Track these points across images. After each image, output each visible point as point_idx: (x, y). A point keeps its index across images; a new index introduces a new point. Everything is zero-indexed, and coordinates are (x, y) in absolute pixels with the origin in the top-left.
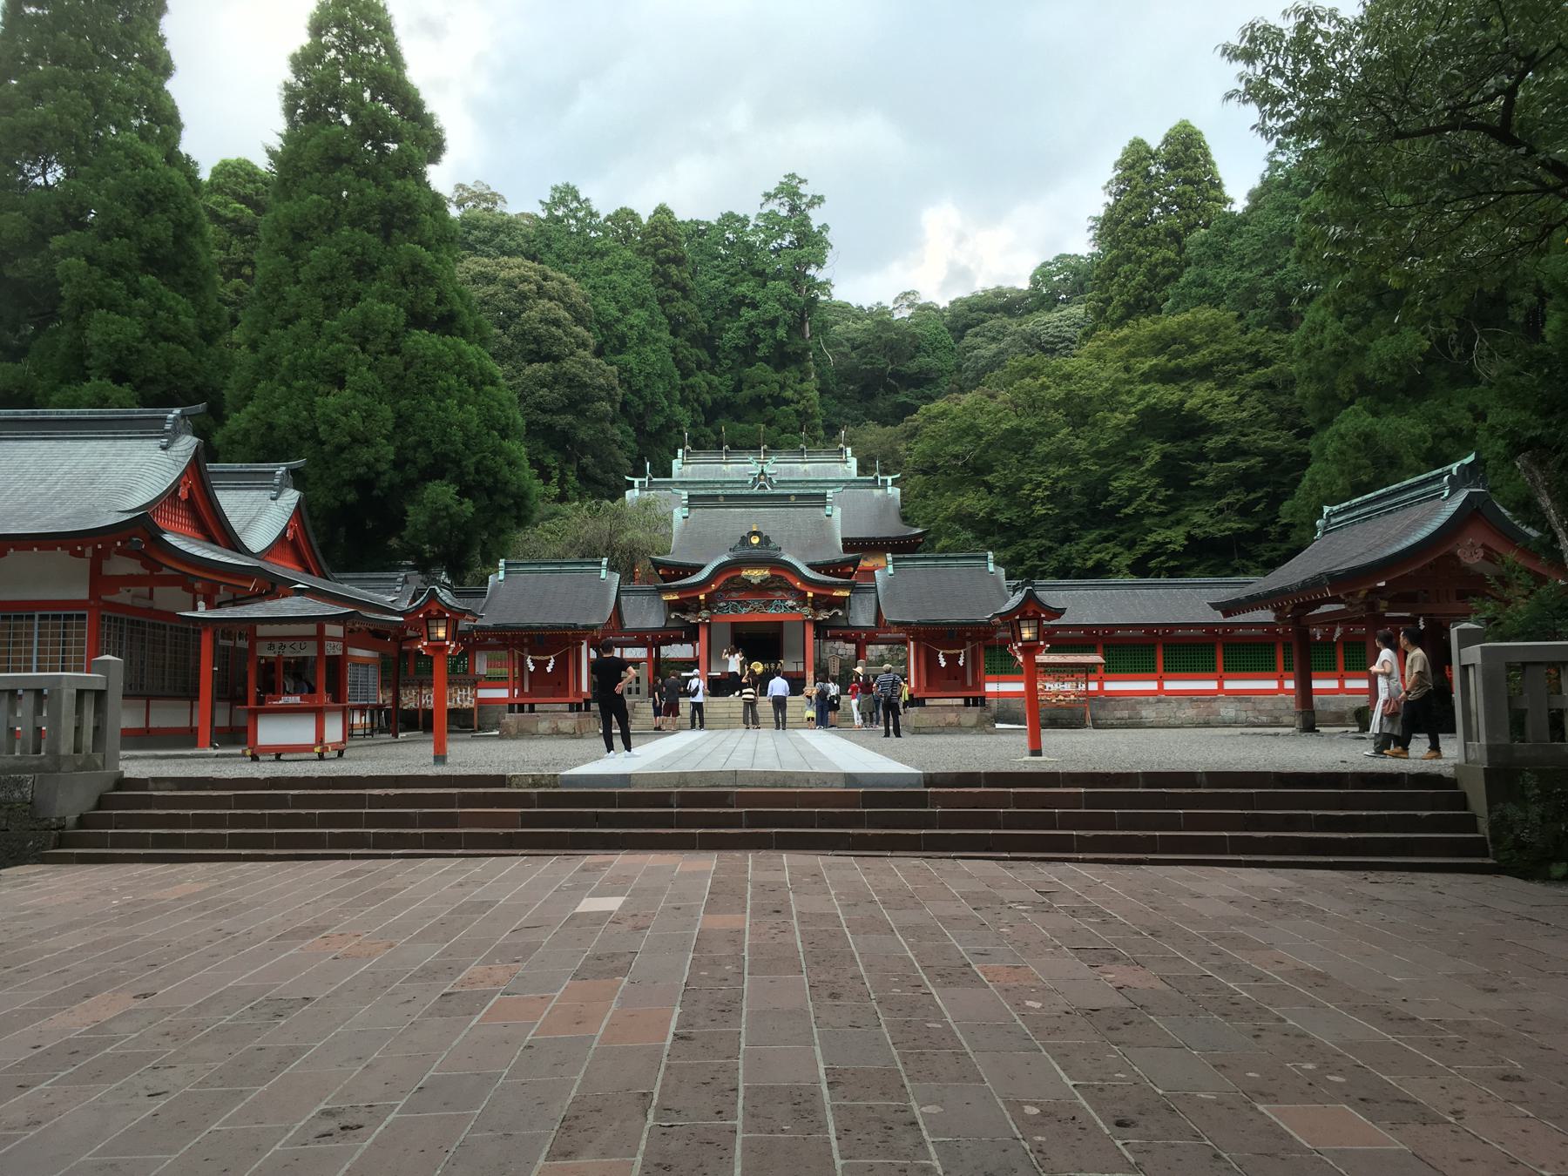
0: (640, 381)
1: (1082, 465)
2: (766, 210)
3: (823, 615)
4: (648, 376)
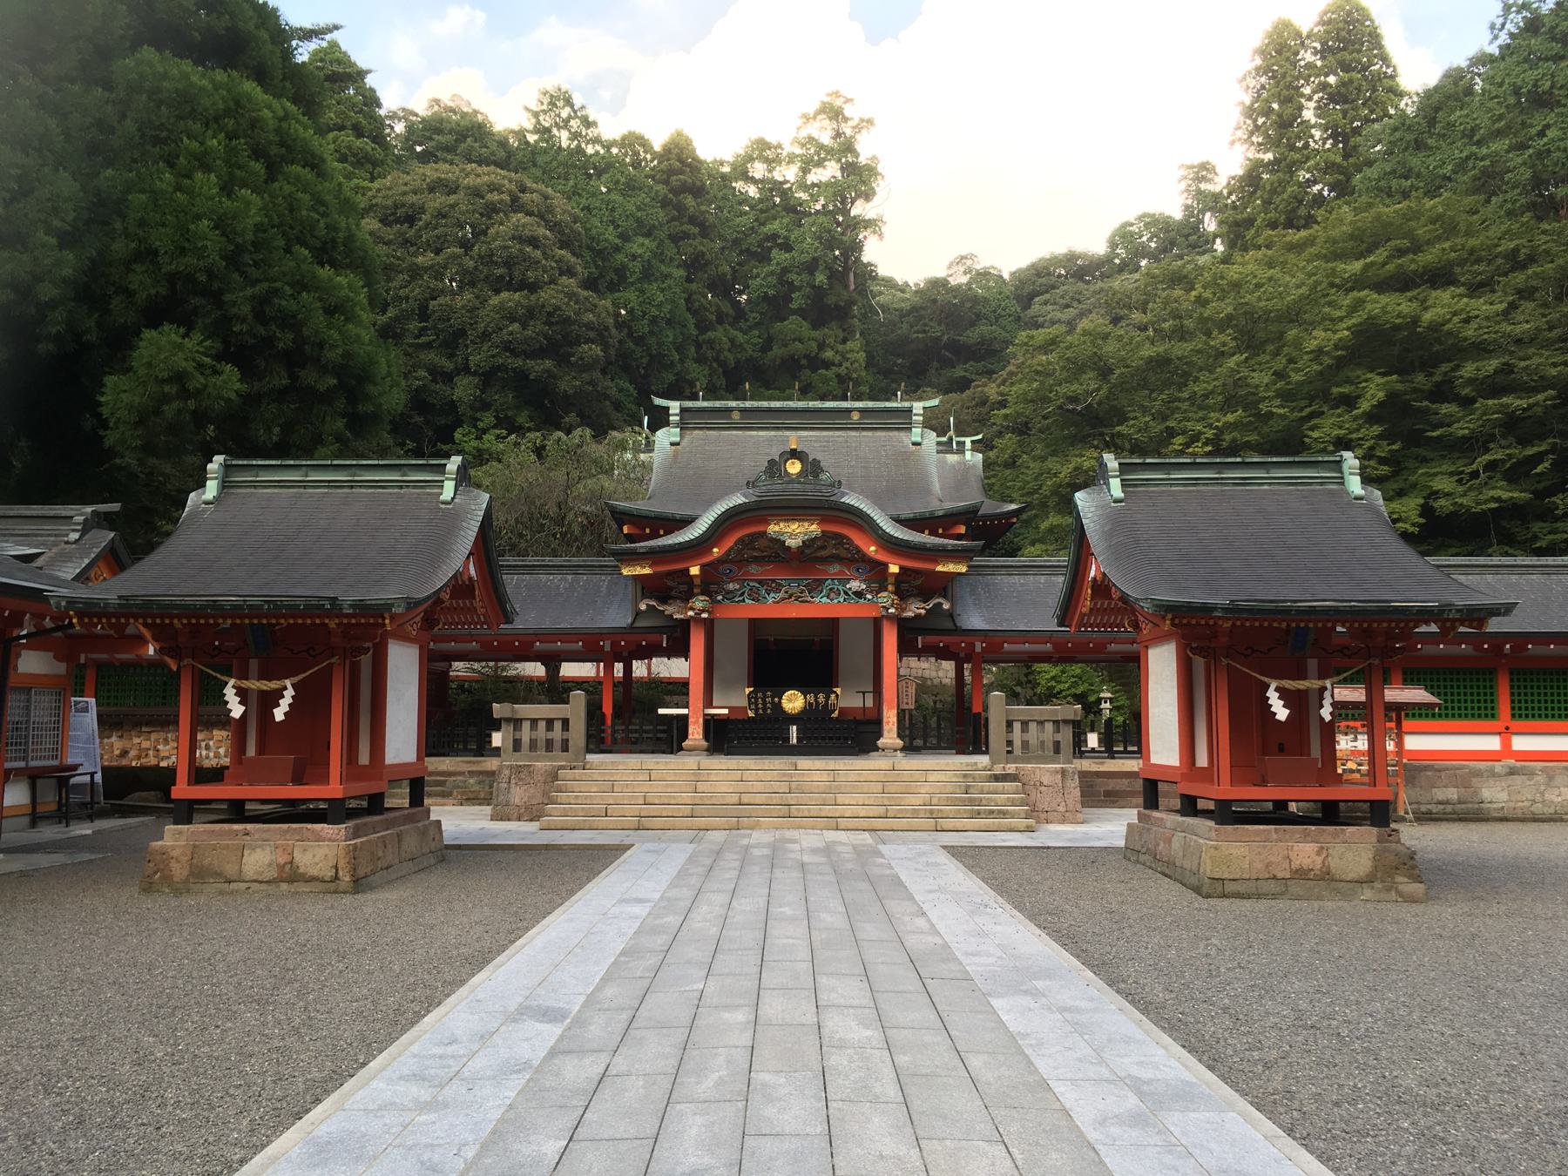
0: (643, 327)
1: (1264, 407)
2: (804, 134)
3: (915, 609)
4: (654, 321)
